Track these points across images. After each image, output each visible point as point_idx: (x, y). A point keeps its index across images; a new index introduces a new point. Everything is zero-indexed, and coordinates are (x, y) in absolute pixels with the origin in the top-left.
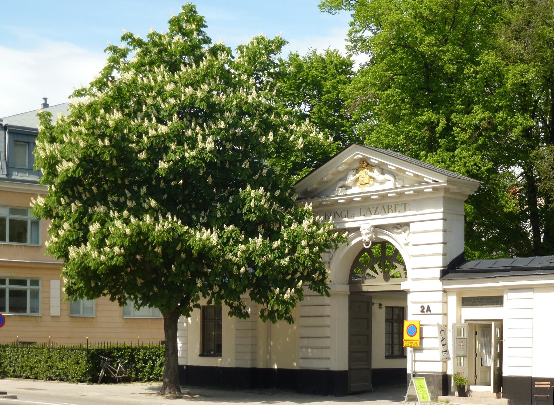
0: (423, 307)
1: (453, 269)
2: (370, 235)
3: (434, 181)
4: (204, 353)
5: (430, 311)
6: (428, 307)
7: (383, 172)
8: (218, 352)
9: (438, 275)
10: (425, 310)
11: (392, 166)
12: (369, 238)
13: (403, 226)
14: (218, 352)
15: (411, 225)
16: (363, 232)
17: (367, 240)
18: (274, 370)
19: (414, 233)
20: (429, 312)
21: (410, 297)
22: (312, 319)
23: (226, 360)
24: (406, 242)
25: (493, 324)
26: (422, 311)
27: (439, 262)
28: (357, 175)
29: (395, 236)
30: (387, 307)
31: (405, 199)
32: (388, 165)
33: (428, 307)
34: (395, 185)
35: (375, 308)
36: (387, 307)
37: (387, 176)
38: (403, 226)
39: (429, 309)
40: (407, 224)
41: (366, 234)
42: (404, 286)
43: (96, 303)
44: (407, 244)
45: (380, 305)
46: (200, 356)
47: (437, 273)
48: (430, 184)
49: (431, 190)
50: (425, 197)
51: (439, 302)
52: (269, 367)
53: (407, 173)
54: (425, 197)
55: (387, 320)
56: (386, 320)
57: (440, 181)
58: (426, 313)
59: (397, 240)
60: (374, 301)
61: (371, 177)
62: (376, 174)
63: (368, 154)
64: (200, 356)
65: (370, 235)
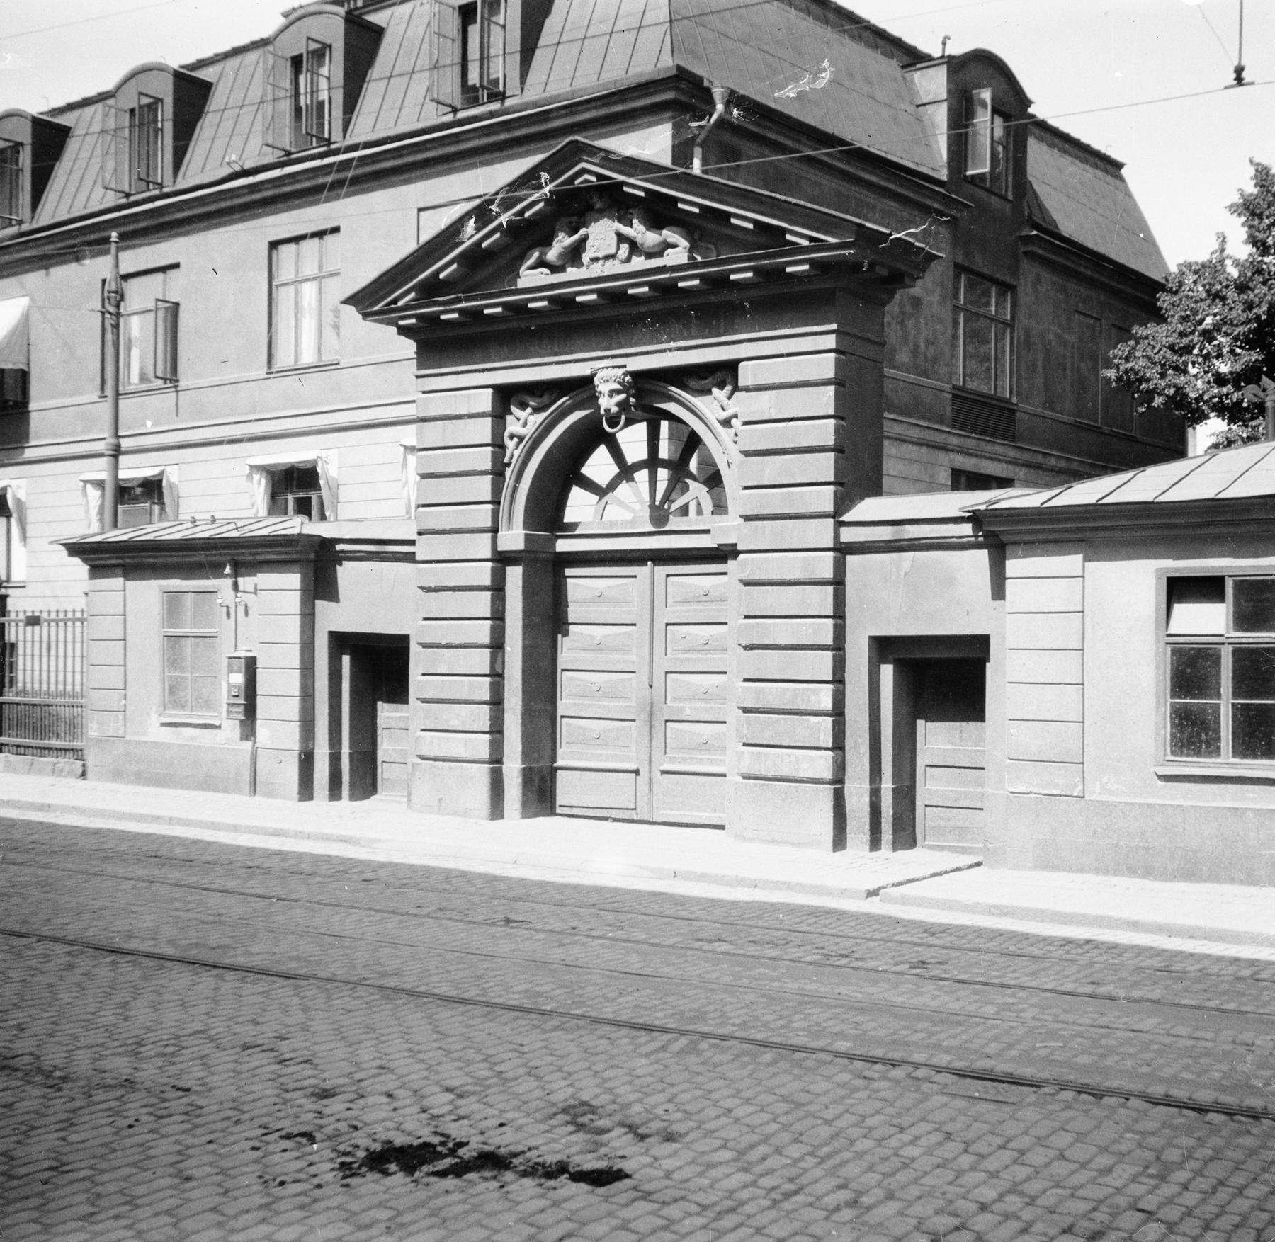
2: (623, 396)
7: (655, 223)
12: (618, 404)
13: (724, 374)
16: (603, 387)
17: (614, 409)
19: (748, 389)
22: (908, 527)
24: (724, 415)
28: (582, 231)
29: (698, 402)
31: (725, 295)
32: (676, 200)
34: (691, 258)
37: (669, 235)
38: (724, 374)
41: (612, 393)
43: (89, 526)
44: (726, 423)
50: (729, 232)
51: (486, 647)
53: (733, 221)
54: (729, 232)
57: (833, 240)
61: (621, 238)
65: (623, 396)
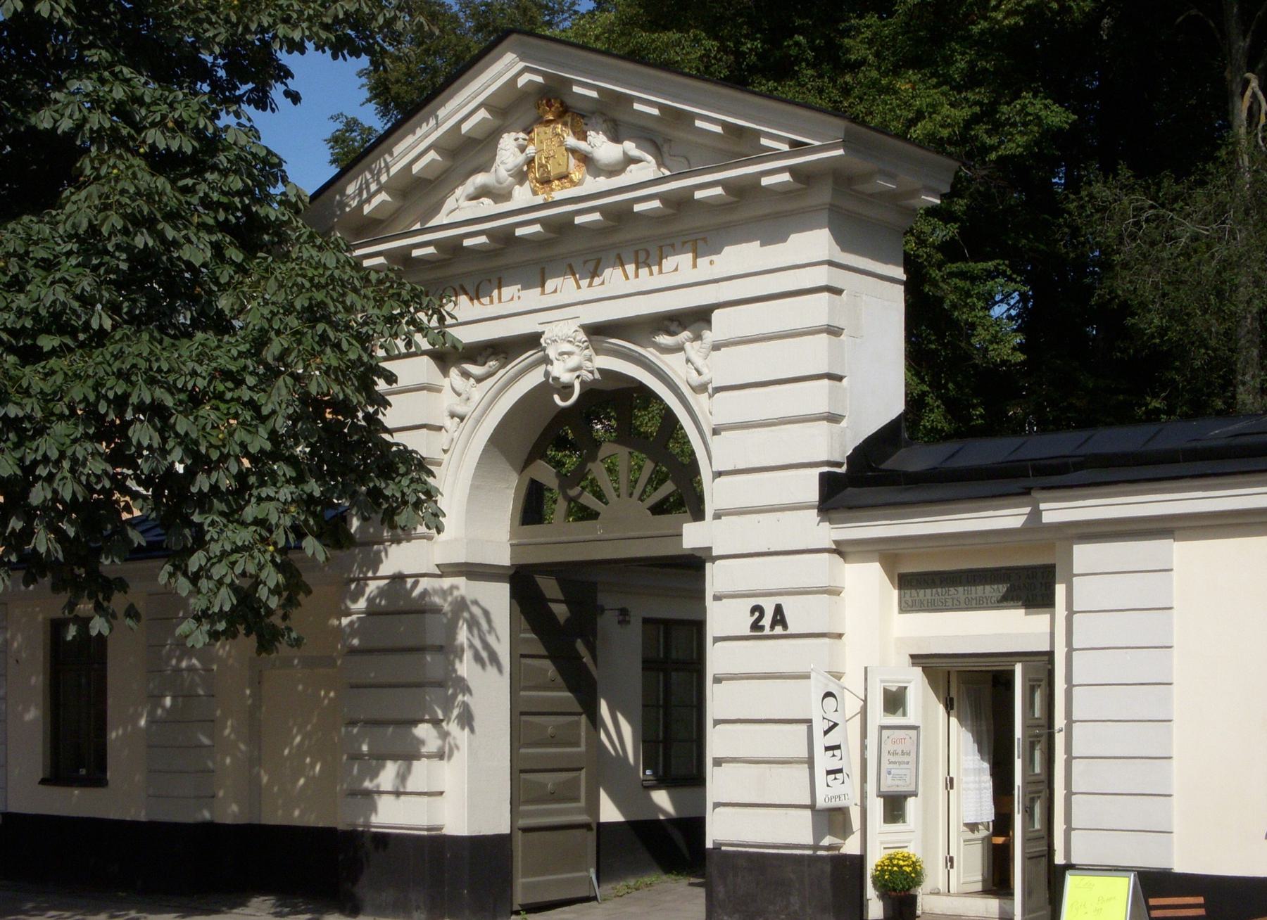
0: (758, 609)
1: (860, 482)
3: (795, 144)
4: (57, 776)
5: (785, 627)
6: (779, 610)
8: (97, 777)
9: (813, 495)
10: (766, 621)
11: (647, 105)
14: (97, 777)
15: (717, 316)
17: (566, 377)
18: (660, 821)
20: (779, 630)
21: (716, 577)
23: (124, 797)
25: (1018, 669)
26: (756, 626)
27: (833, 446)
30: (646, 621)
33: (779, 610)
35: (608, 622)
36: (646, 621)
39: (779, 618)
40: (698, 318)
42: (693, 536)
45: (624, 612)
46: (44, 782)
47: (808, 487)
48: (781, 155)
49: (786, 177)
52: (256, 822)
55: (649, 665)
56: (645, 661)
57: (817, 143)
58: (767, 631)
59: (675, 369)
60: (604, 599)
62: (602, 147)
63: (617, 83)
64: (44, 782)
